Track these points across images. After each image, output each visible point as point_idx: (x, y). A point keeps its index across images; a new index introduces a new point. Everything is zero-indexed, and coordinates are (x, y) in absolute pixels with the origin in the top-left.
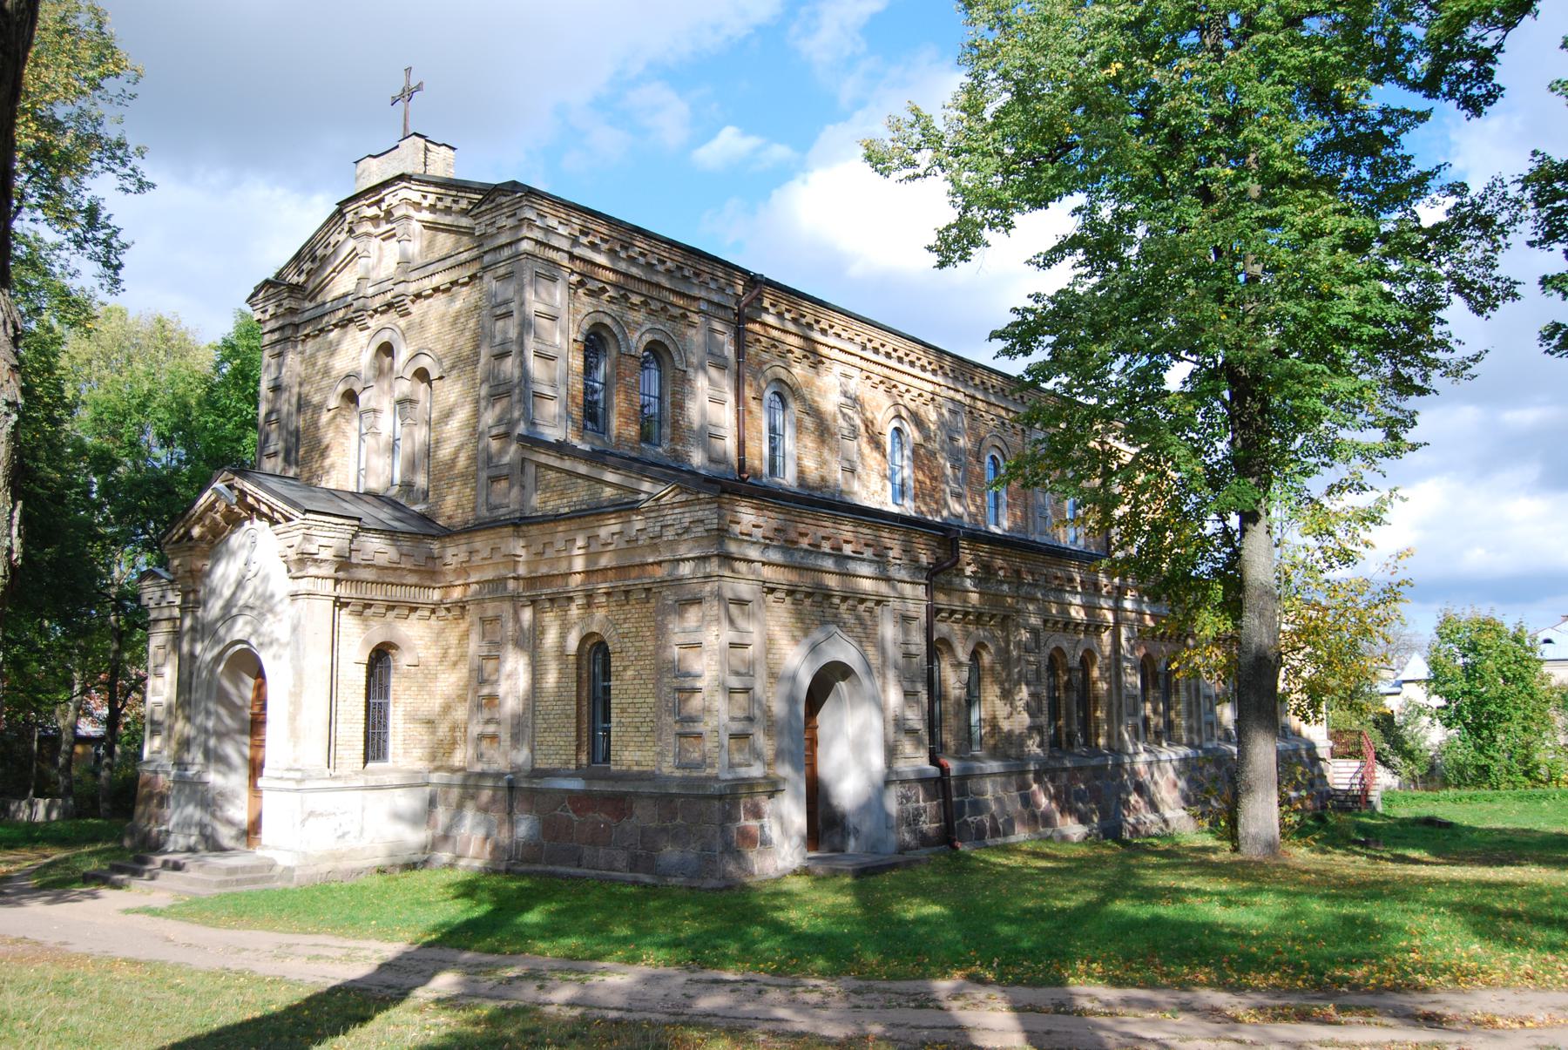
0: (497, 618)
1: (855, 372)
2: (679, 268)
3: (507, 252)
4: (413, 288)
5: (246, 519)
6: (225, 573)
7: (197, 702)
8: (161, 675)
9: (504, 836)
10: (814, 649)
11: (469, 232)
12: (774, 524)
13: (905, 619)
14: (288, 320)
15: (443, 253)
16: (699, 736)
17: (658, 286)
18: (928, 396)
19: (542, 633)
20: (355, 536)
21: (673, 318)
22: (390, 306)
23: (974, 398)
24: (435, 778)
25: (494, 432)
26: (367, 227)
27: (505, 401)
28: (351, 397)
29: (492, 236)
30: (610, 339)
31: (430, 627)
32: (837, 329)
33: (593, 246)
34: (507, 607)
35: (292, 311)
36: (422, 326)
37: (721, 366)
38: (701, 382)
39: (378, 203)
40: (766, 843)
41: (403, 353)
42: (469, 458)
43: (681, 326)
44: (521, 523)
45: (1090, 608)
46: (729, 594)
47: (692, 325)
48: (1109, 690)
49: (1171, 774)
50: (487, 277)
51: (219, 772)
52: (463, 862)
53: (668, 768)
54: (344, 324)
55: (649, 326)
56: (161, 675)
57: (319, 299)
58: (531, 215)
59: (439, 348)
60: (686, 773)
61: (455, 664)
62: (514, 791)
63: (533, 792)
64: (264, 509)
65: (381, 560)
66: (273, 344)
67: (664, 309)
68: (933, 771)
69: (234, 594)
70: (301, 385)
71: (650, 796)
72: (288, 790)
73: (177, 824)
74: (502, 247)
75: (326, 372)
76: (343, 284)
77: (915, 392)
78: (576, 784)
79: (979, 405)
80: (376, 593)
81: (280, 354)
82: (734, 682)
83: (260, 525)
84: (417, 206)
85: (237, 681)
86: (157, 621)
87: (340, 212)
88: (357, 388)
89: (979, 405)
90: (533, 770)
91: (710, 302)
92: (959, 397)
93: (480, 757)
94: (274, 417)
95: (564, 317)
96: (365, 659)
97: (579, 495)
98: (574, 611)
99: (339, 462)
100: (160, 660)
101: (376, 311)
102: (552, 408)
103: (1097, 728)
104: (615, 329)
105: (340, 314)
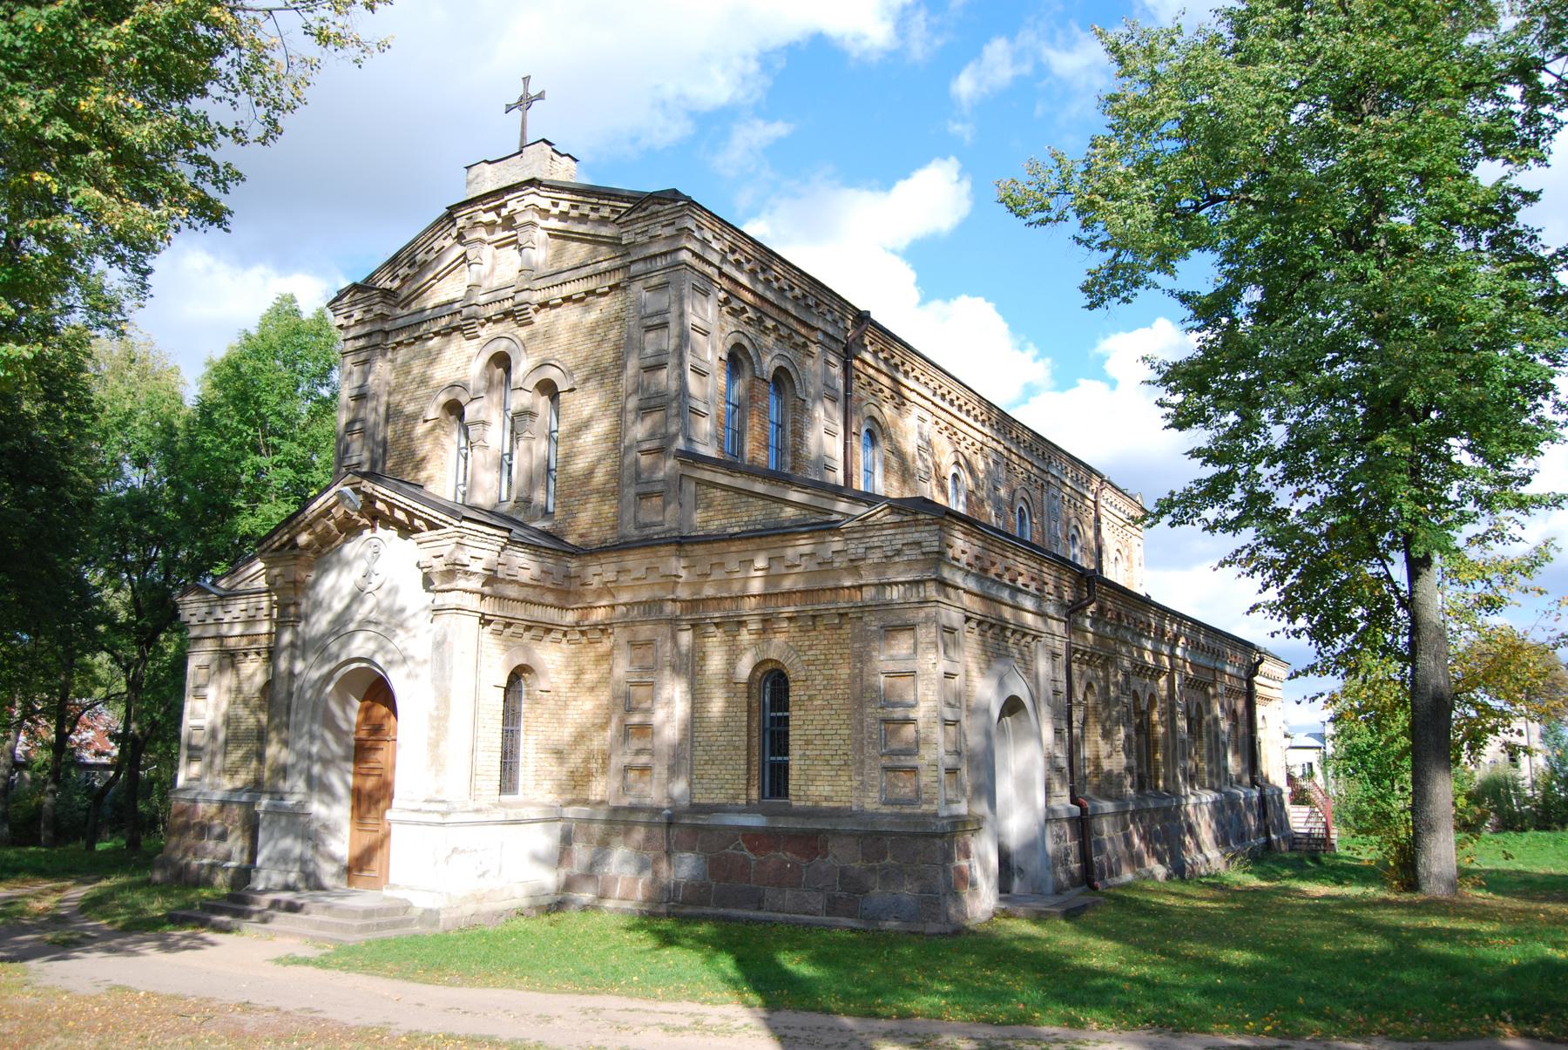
0: (649, 643)
1: (927, 416)
2: (804, 297)
3: (660, 263)
4: (538, 297)
5: (366, 527)
6: (335, 586)
7: (298, 726)
8: (204, 697)
9: (666, 873)
10: (1001, 684)
11: (614, 243)
12: (976, 550)
13: (1054, 655)
14: (378, 326)
15: (576, 262)
16: (914, 770)
17: (786, 312)
18: (978, 445)
19: (703, 659)
20: (503, 549)
21: (795, 346)
22: (507, 314)
23: (1009, 450)
24: (570, 812)
25: (646, 446)
26: (481, 233)
27: (657, 416)
28: (454, 409)
29: (643, 245)
30: (746, 364)
31: (561, 650)
32: (917, 373)
33: (738, 264)
34: (665, 630)
35: (383, 317)
36: (548, 336)
37: (834, 400)
38: (819, 412)
39: (497, 209)
40: (973, 884)
41: (523, 367)
42: (607, 473)
43: (800, 355)
44: (681, 542)
45: (1157, 654)
46: (944, 621)
47: (810, 355)
48: (1165, 734)
49: (1207, 816)
50: (637, 286)
51: (322, 802)
52: (609, 904)
53: (871, 802)
54: (447, 333)
55: (777, 352)
56: (204, 697)
57: (414, 306)
58: (691, 224)
59: (570, 361)
60: (896, 809)
61: (592, 689)
62: (676, 827)
63: (696, 828)
64: (400, 515)
65: (524, 576)
66: (357, 351)
67: (790, 337)
68: (1076, 809)
69: (348, 607)
70: (390, 394)
71: (851, 834)
72: (428, 824)
73: (269, 859)
74: (655, 256)
75: (424, 381)
76: (446, 290)
77: (970, 441)
78: (755, 821)
79: (1014, 457)
80: (520, 612)
81: (365, 362)
82: (949, 715)
83: (387, 537)
84: (545, 213)
85: (344, 703)
86: (198, 639)
87: (450, 215)
88: (463, 399)
89: (1014, 457)
90: (692, 805)
91: (825, 333)
92: (1000, 448)
93: (626, 789)
94: (358, 426)
95: (715, 333)
96: (504, 683)
97: (756, 513)
98: (745, 636)
99: (438, 475)
100: (200, 681)
101: (489, 320)
102: (705, 426)
103: (1157, 770)
104: (751, 351)
105: (444, 322)
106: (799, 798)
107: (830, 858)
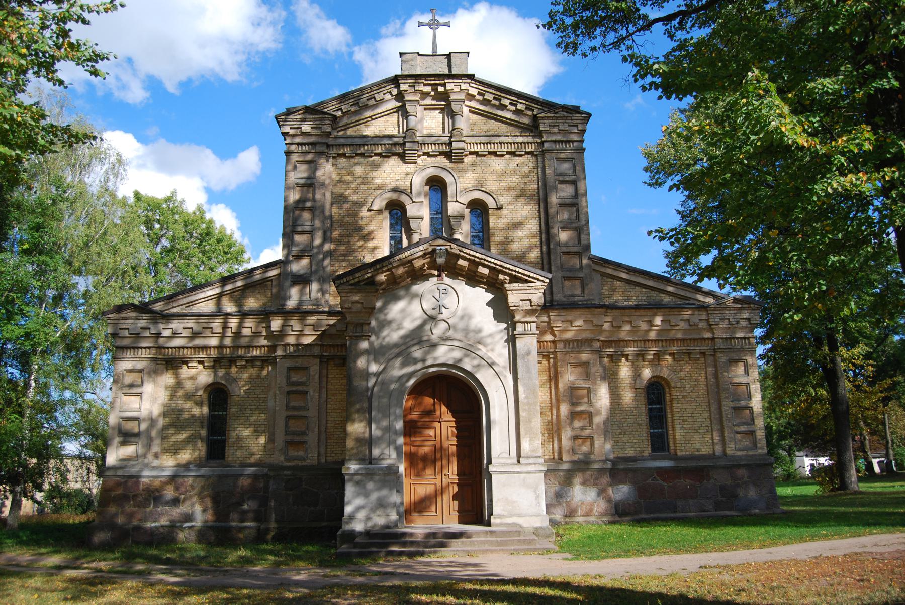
5: (433, 275)
29: (554, 133)
54: (385, 156)
60: (744, 453)
62: (617, 470)
106: (681, 451)
107: (712, 481)
